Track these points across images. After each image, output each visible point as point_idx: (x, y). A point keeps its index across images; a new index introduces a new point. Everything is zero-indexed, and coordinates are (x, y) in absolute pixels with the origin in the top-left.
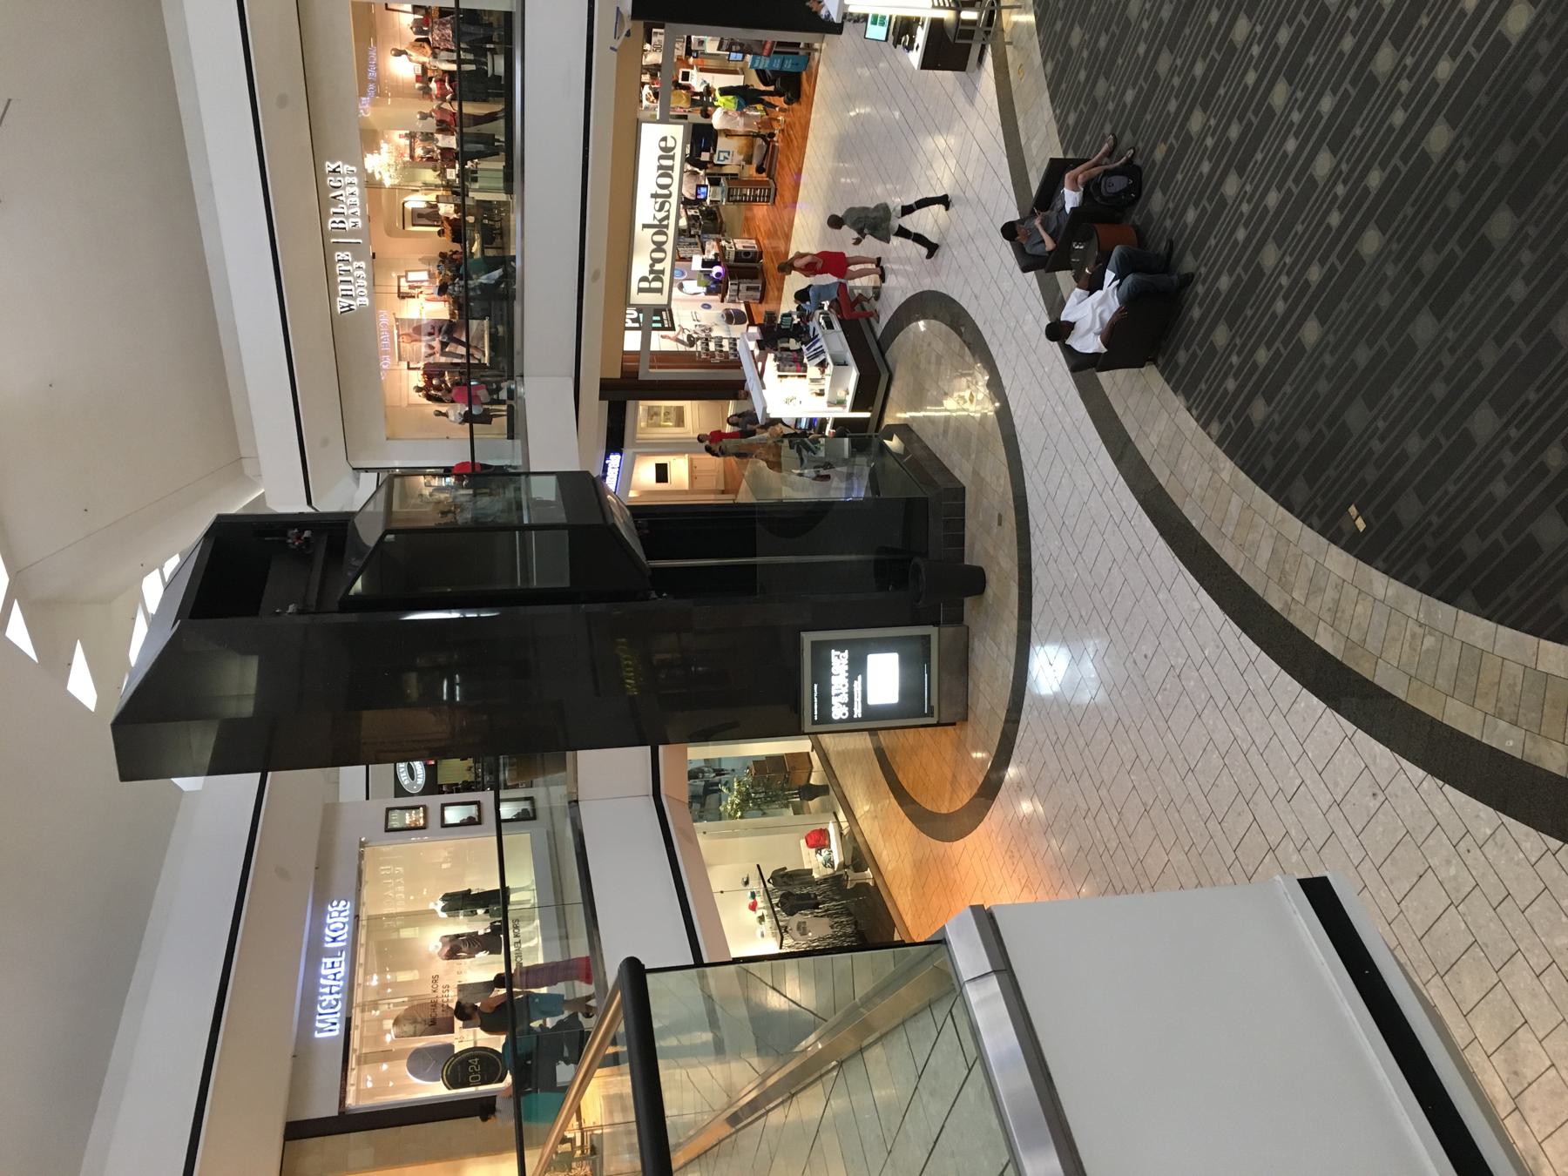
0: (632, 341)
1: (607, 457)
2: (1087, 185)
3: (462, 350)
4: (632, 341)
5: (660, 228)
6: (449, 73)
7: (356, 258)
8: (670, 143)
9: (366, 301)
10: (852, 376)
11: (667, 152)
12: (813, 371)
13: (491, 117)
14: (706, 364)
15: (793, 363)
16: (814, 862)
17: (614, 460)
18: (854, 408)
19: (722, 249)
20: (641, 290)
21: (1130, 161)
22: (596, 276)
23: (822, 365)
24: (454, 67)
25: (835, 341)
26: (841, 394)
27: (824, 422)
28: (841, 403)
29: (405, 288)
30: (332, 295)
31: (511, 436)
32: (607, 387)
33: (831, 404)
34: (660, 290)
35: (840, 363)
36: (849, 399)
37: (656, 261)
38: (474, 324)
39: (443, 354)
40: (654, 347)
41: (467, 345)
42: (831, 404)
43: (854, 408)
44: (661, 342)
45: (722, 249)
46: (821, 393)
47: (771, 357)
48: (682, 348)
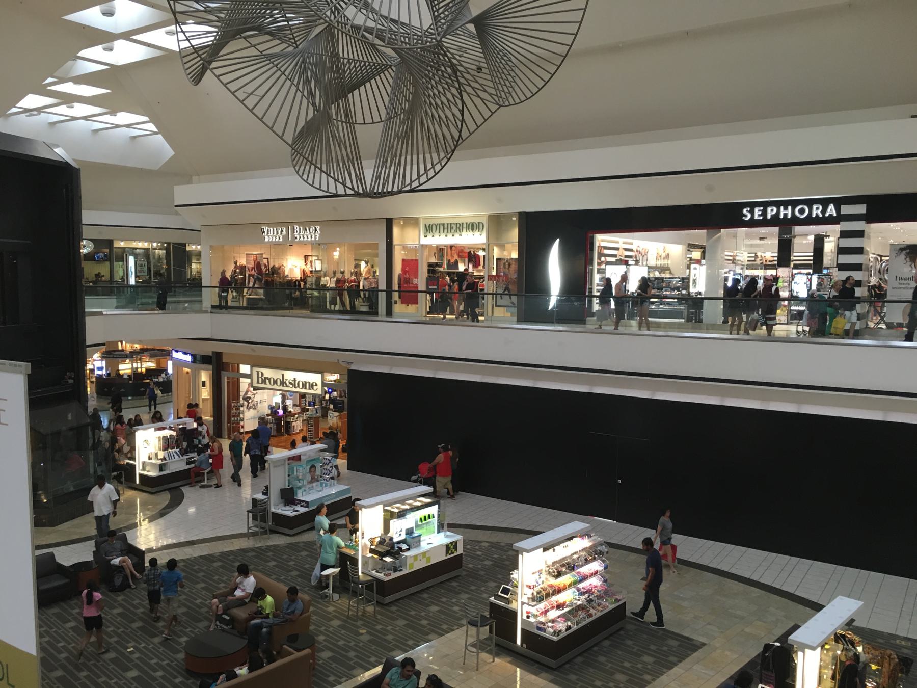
0: (245, 369)
1: (192, 355)
2: (122, 567)
3: (251, 285)
4: (245, 369)
5: (283, 383)
6: (359, 286)
7: (284, 237)
8: (315, 388)
9: (267, 240)
10: (153, 473)
11: (311, 386)
12: (161, 454)
13: (343, 304)
14: (229, 408)
15: (167, 444)
16: (657, 546)
17: (188, 358)
18: (141, 475)
19: (294, 415)
20: (258, 372)
21: (130, 586)
22: (253, 350)
23: (164, 459)
24: (361, 288)
25: (178, 464)
26: (148, 468)
27: (134, 459)
28: (144, 469)
29: (310, 259)
30: (270, 224)
31: (213, 307)
32: (219, 355)
33: (144, 463)
34: (258, 382)
35: (161, 468)
36: (145, 473)
37: (270, 380)
38: (262, 291)
39: (250, 275)
40: (242, 380)
41: (253, 287)
42: (144, 463)
43: (141, 475)
44: (244, 383)
45: (294, 415)
46: (150, 458)
47: (174, 433)
48: (242, 394)
